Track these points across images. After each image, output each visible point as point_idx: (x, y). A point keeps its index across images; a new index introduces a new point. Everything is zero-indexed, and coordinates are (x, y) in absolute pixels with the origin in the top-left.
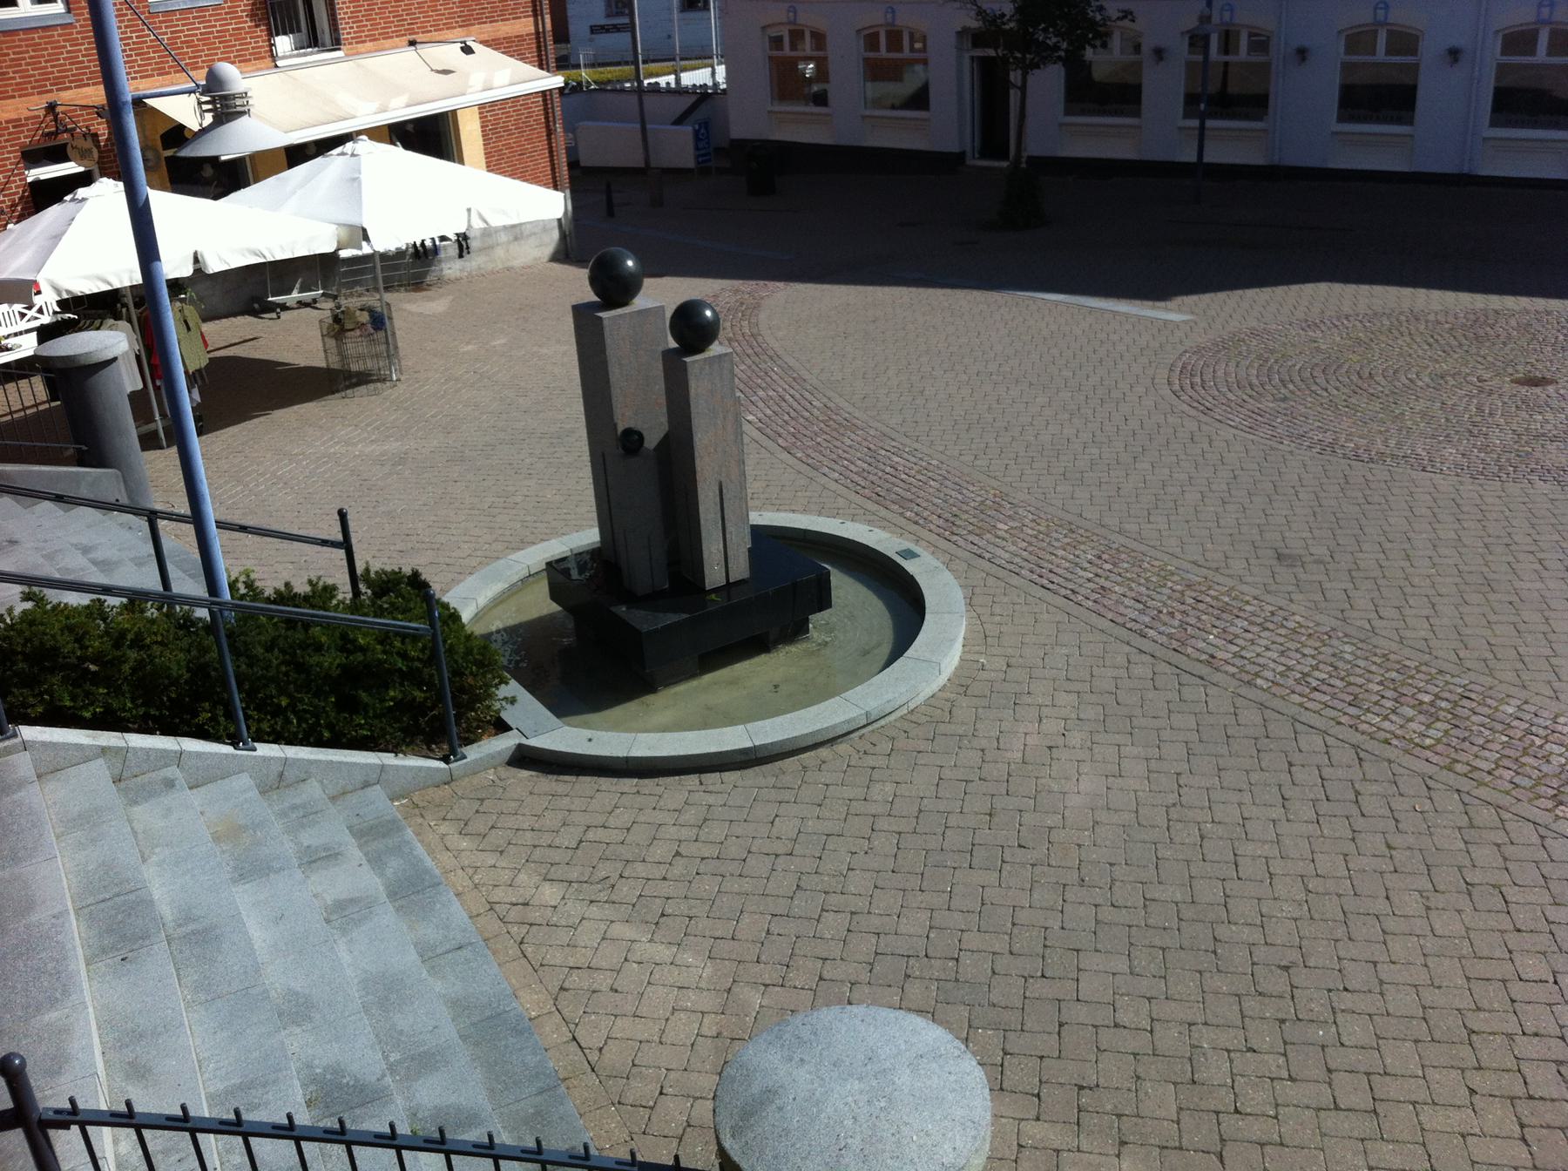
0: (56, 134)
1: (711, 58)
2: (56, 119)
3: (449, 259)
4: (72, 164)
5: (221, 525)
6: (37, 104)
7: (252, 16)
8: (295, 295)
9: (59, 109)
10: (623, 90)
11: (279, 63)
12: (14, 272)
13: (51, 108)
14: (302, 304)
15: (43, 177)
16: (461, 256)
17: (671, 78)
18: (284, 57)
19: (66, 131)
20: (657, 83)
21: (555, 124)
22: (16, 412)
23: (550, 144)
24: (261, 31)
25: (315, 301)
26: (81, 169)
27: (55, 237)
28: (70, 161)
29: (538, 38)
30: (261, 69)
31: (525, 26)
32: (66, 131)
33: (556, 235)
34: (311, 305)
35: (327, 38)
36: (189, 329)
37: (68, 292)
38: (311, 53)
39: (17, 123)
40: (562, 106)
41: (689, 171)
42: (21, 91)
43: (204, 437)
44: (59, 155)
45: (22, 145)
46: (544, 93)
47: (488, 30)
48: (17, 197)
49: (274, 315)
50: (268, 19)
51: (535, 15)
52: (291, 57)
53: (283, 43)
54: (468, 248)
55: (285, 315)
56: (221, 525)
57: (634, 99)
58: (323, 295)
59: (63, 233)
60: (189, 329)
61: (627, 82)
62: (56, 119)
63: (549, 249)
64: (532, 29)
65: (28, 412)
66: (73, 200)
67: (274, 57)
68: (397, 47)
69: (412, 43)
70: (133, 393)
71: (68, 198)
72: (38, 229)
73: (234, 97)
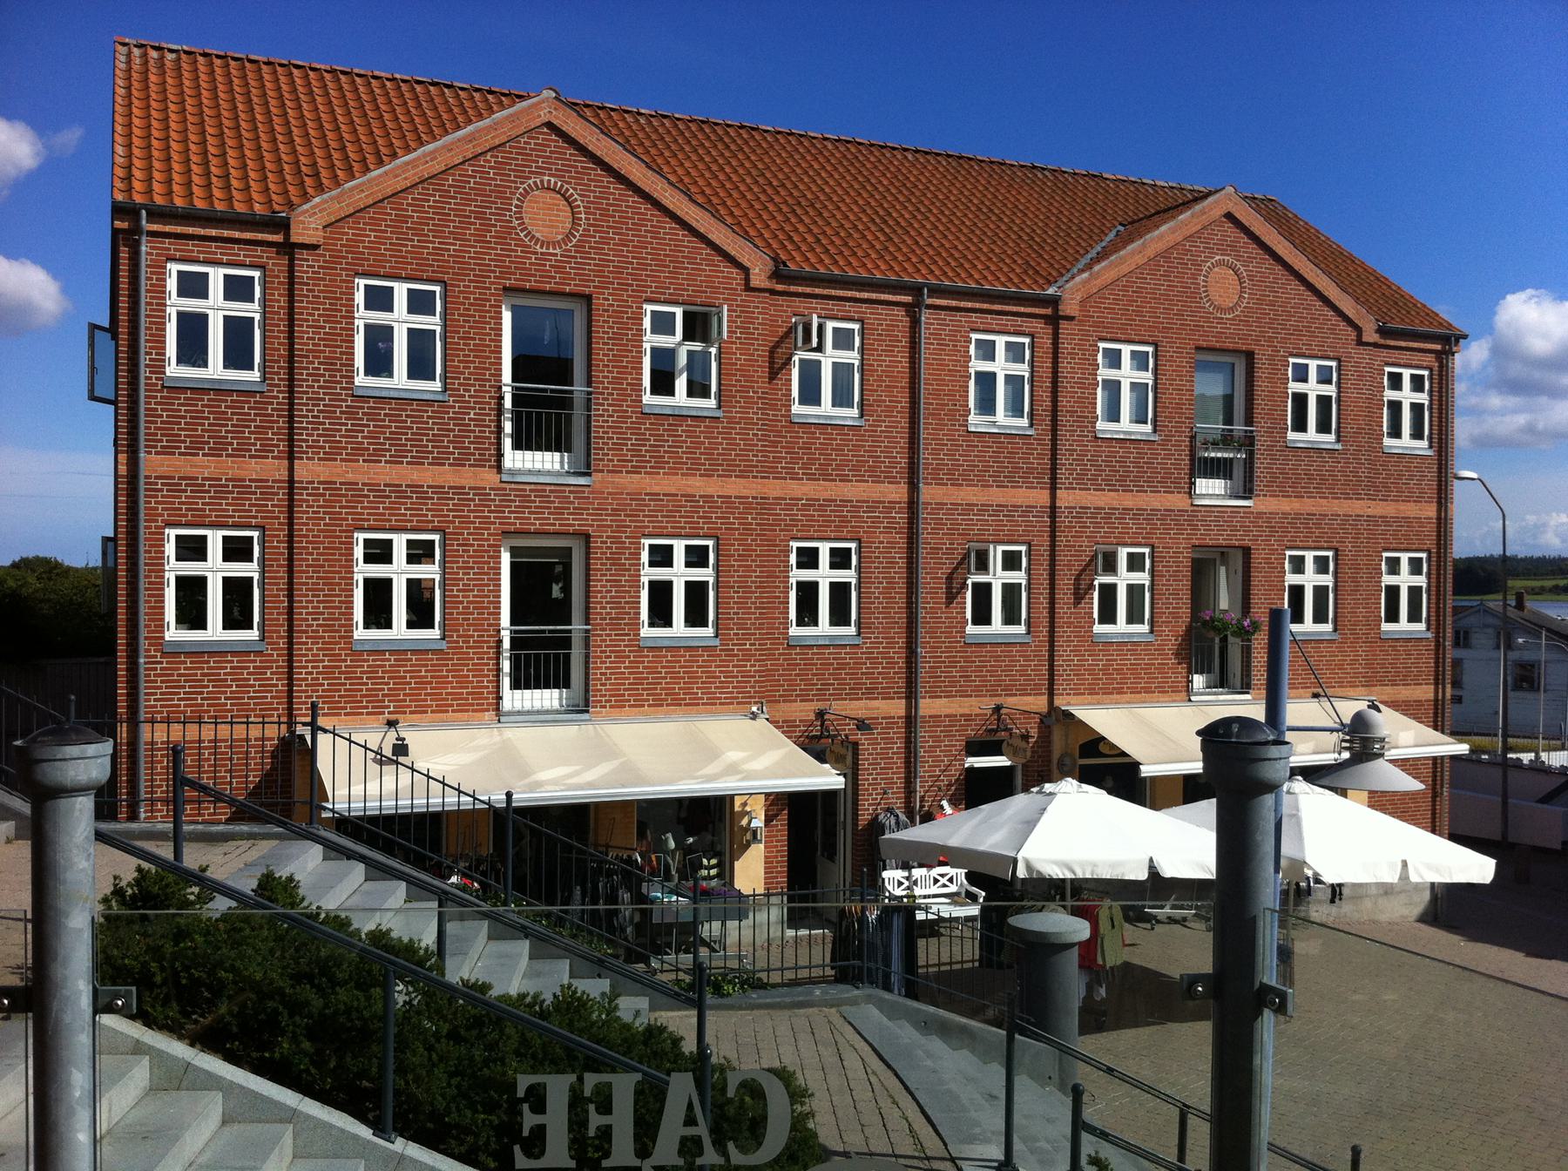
0: (995, 731)
1: (1537, 738)
2: (999, 720)
3: (1320, 902)
4: (1004, 758)
5: (1272, 1147)
6: (988, 704)
7: (1177, 655)
8: (1167, 910)
9: (1003, 711)
10: (1480, 761)
11: (1193, 698)
12: (991, 846)
13: (998, 709)
14: (1172, 920)
15: (976, 765)
16: (1332, 901)
17: (1532, 756)
18: (1197, 694)
19: (1006, 730)
20: (1518, 759)
21: (1442, 787)
22: (945, 964)
23: (1434, 805)
24: (1182, 669)
25: (1185, 919)
26: (1008, 763)
27: (1028, 822)
28: (1001, 754)
29: (1436, 706)
30: (1174, 701)
31: (1426, 692)
32: (1006, 730)
33: (1427, 896)
34: (1182, 922)
35: (1238, 683)
36: (1113, 927)
37: (1038, 872)
38: (1222, 694)
39: (968, 717)
40: (1451, 767)
41: (1554, 852)
42: (978, 692)
43: (534, 962)
44: (993, 749)
45: (968, 736)
46: (1435, 759)
47: (1389, 692)
48: (953, 779)
49: (1148, 926)
50: (1190, 659)
51: (1436, 684)
52: (1202, 694)
53: (1198, 681)
54: (1341, 894)
55: (1158, 928)
56: (1272, 1147)
57: (1497, 773)
58: (1195, 915)
59: (1038, 820)
60: (1113, 927)
61: (1484, 752)
62: (999, 720)
63: (1417, 910)
64: (1431, 696)
65: (930, 970)
66: (1039, 792)
67: (1189, 690)
68: (1300, 697)
69: (1316, 696)
70: (290, 884)
71: (1035, 790)
72: (1009, 812)
73: (1374, 740)
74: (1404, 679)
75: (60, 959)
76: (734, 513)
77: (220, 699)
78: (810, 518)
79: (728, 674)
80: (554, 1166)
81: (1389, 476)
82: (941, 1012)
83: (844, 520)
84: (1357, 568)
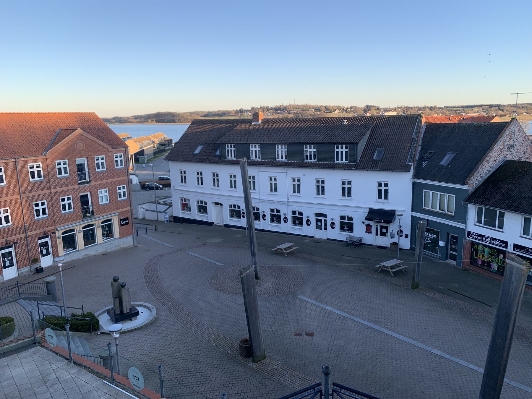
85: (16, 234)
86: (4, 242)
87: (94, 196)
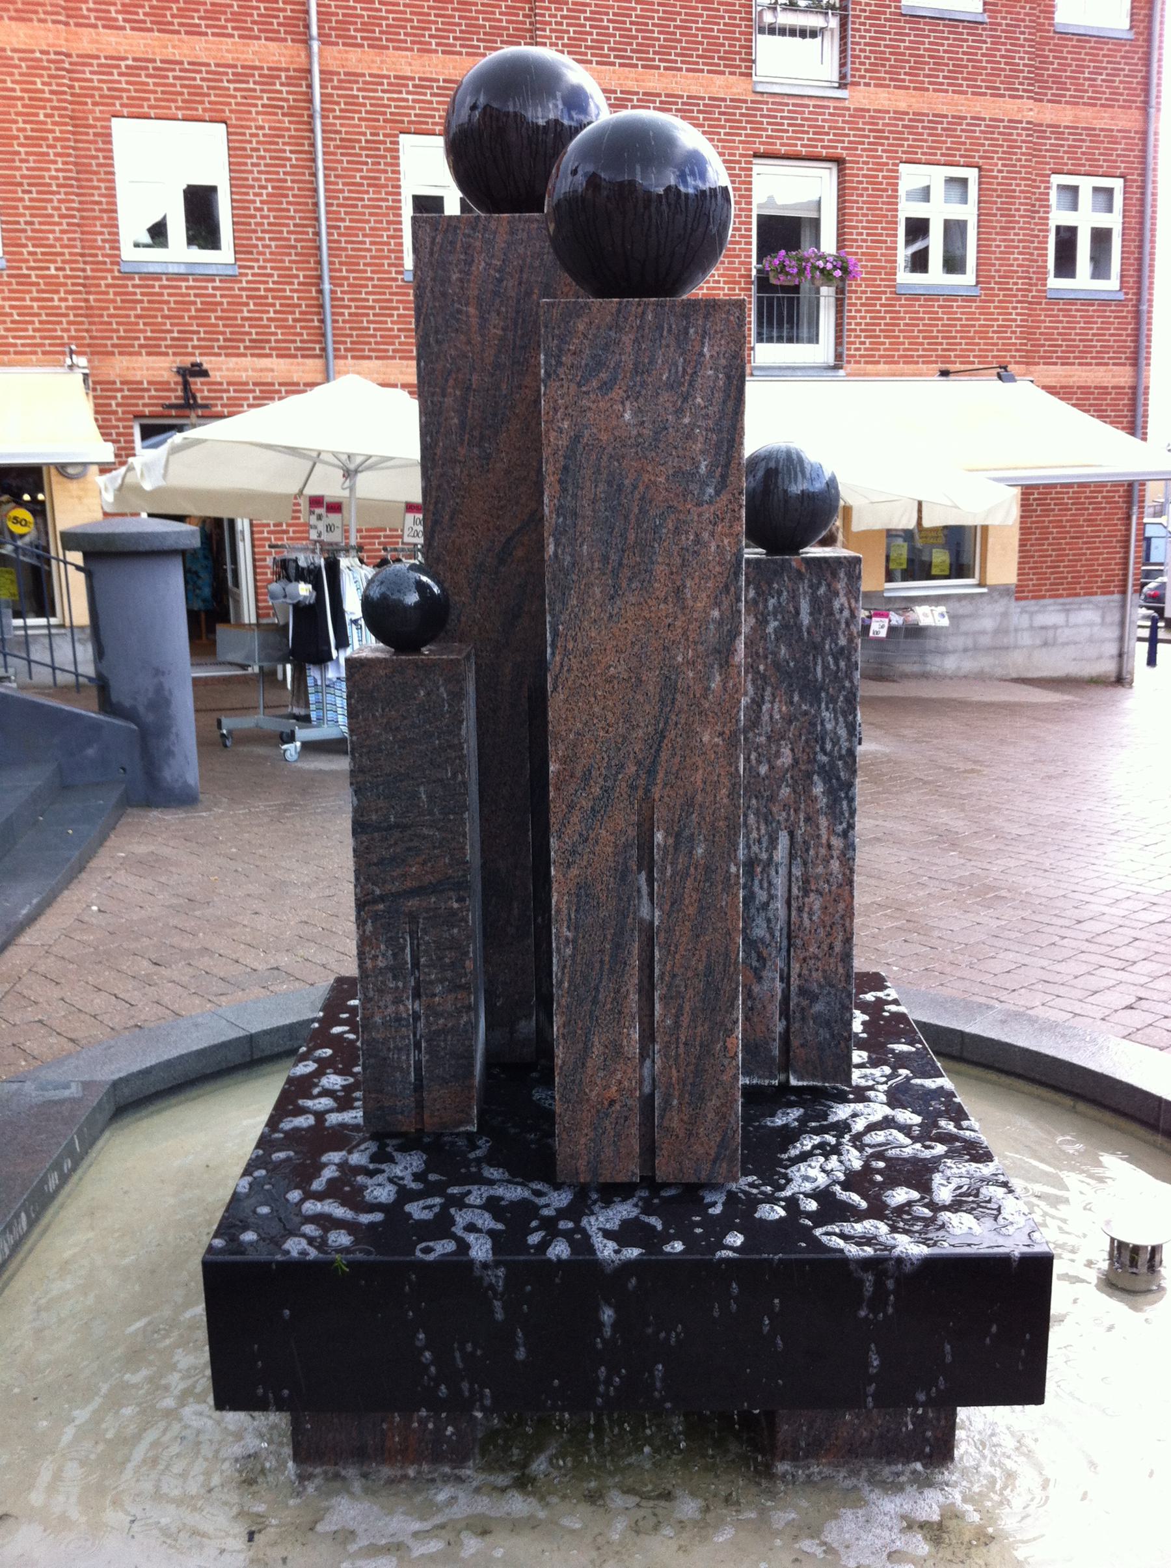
69: (945, 373)
74: (1082, 355)
75: (138, 1116)
76: (12, 74)
77: (399, 34)
78: (142, 88)
79: (24, 311)
80: (1049, 1360)
81: (1063, 67)
82: (67, 708)
83: (196, 91)
84: (1010, 194)
85: (258, 348)
86: (162, 386)
87: (859, 202)
